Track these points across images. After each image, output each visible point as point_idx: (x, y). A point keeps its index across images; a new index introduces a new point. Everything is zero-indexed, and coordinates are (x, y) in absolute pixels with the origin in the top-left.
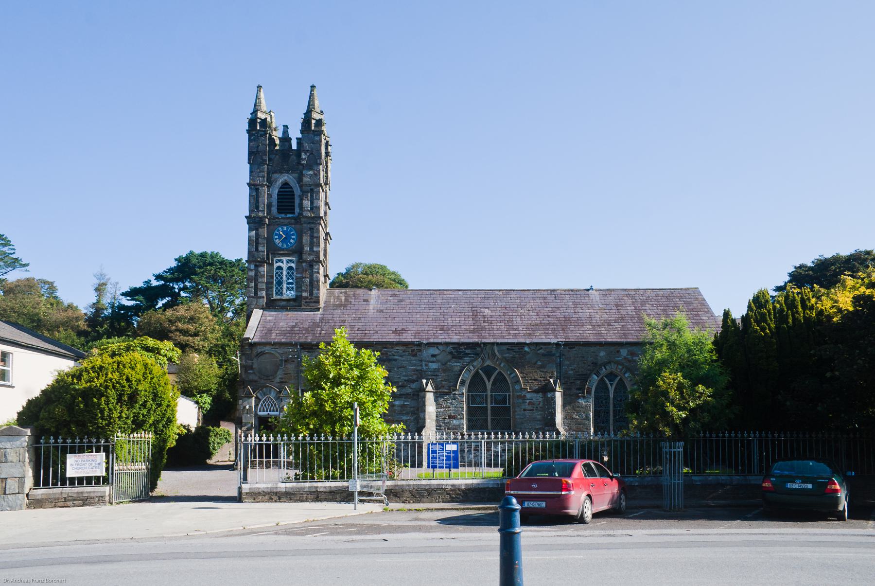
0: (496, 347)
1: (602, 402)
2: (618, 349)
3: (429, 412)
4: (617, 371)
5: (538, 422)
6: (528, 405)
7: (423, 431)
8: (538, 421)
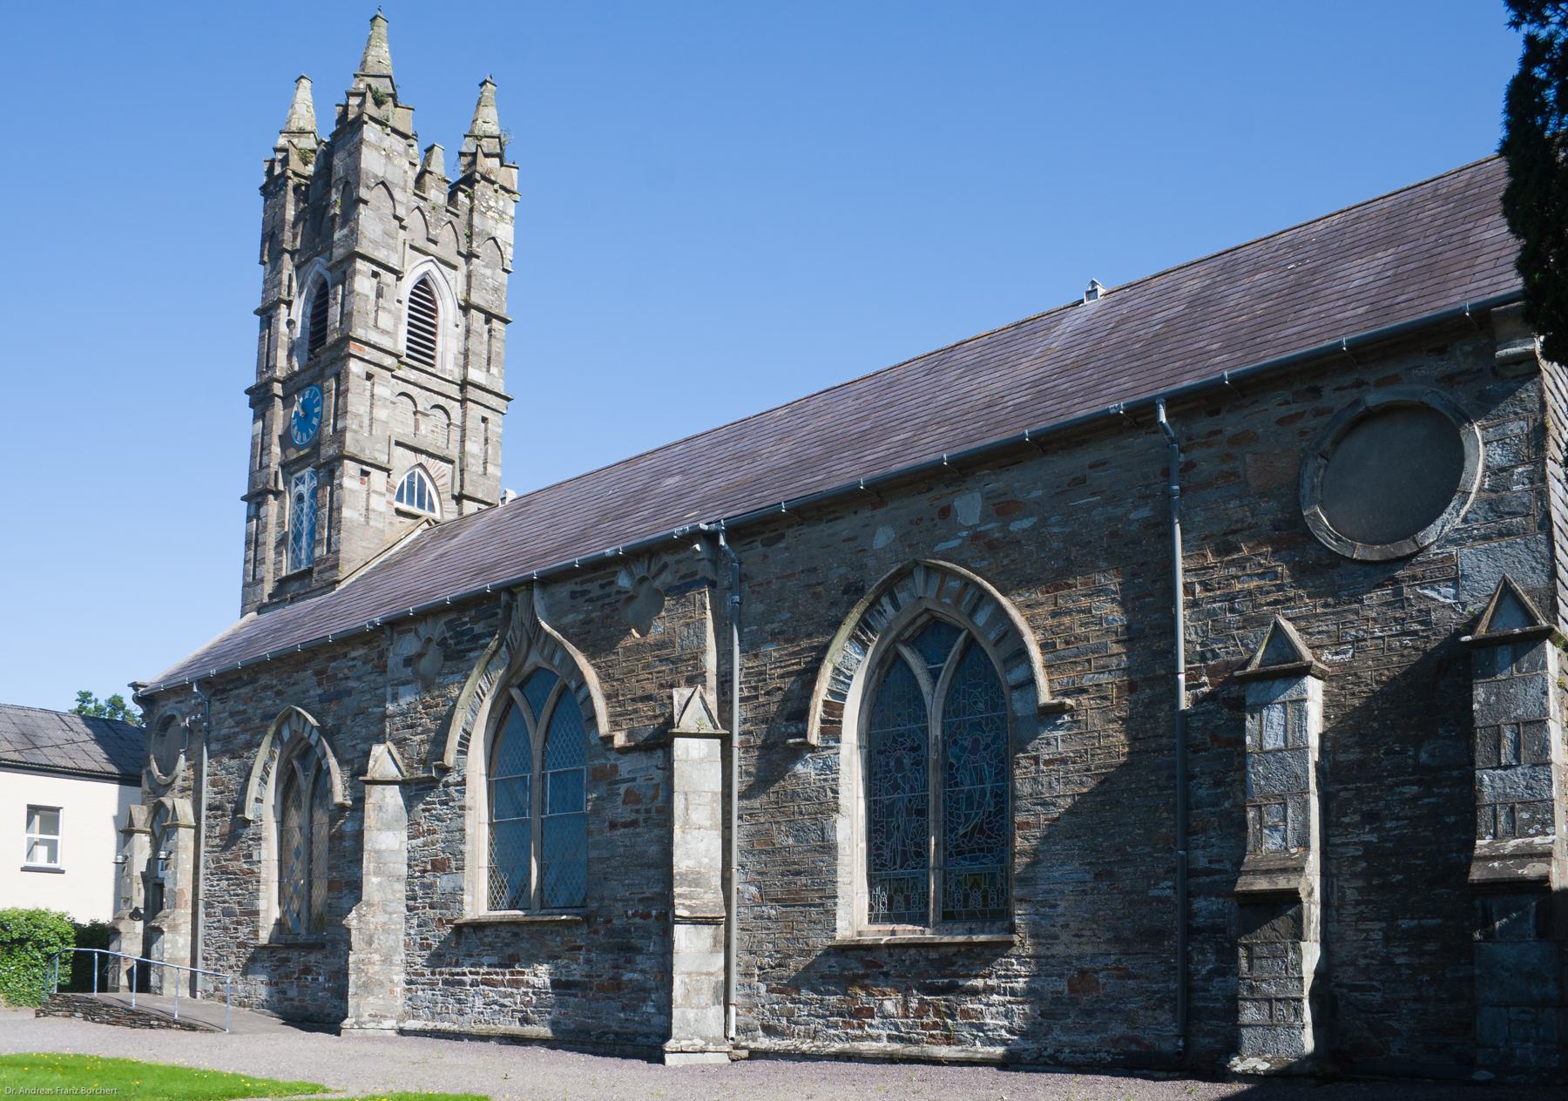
0: (536, 593)
1: (899, 762)
2: (943, 503)
3: (378, 852)
4: (942, 605)
5: (652, 872)
6: (624, 803)
7: (353, 914)
8: (649, 866)
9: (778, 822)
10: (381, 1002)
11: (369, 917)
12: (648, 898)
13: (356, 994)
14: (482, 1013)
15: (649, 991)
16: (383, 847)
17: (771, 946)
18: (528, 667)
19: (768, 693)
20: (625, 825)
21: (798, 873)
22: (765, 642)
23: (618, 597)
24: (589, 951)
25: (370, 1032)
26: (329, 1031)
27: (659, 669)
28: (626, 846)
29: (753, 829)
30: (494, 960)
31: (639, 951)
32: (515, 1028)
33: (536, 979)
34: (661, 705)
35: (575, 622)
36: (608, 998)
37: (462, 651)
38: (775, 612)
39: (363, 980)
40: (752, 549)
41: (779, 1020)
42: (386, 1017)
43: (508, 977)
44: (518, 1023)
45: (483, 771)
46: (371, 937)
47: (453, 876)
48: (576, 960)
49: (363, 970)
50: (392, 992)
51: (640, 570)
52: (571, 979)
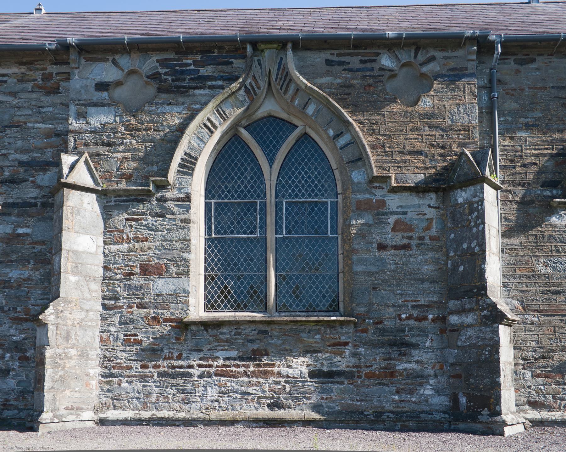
3: (76, 252)
5: (427, 285)
6: (393, 230)
8: (424, 281)
9: (537, 256)
10: (77, 395)
11: (66, 313)
12: (422, 305)
13: (53, 388)
14: (217, 401)
15: (427, 377)
16: (81, 249)
17: (534, 343)
18: (261, 113)
19: (524, 166)
20: (396, 248)
21: (558, 293)
22: (520, 129)
23: (381, 73)
24: (356, 346)
25: (69, 425)
26: (494, 434)
27: (428, 133)
28: (397, 264)
29: (514, 259)
30: (234, 354)
31: (415, 346)
32: (265, 412)
33: (290, 371)
34: (431, 160)
35: (332, 83)
36: (380, 384)
37: (184, 87)
38: (528, 111)
39: (60, 374)
40: (505, 64)
41: (545, 397)
42: (82, 409)
43: (252, 369)
44: (266, 408)
45: (203, 193)
46: (68, 333)
47: (175, 280)
48: (341, 354)
49: (60, 365)
50: (87, 385)
51: (405, 56)
52: (335, 369)
